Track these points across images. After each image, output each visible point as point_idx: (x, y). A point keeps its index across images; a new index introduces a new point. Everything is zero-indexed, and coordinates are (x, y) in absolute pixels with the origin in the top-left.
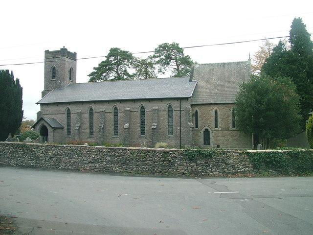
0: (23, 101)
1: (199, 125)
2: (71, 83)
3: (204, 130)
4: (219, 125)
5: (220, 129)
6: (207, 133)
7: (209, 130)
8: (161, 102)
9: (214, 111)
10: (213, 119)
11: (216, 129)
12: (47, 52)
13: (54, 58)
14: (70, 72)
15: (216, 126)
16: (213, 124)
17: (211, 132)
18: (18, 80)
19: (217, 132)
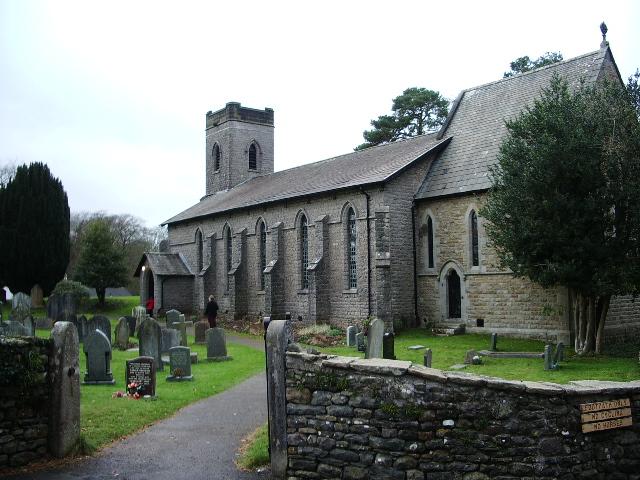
0: (68, 195)
1: (436, 261)
2: (255, 175)
3: (445, 273)
4: (481, 258)
5: (484, 269)
6: (453, 280)
7: (459, 273)
8: (333, 202)
9: (468, 214)
10: (466, 239)
11: (475, 269)
12: (209, 115)
13: (215, 125)
14: (217, 166)
15: (476, 263)
16: (467, 255)
17: (462, 277)
18: (375, 123)
19: (477, 280)
